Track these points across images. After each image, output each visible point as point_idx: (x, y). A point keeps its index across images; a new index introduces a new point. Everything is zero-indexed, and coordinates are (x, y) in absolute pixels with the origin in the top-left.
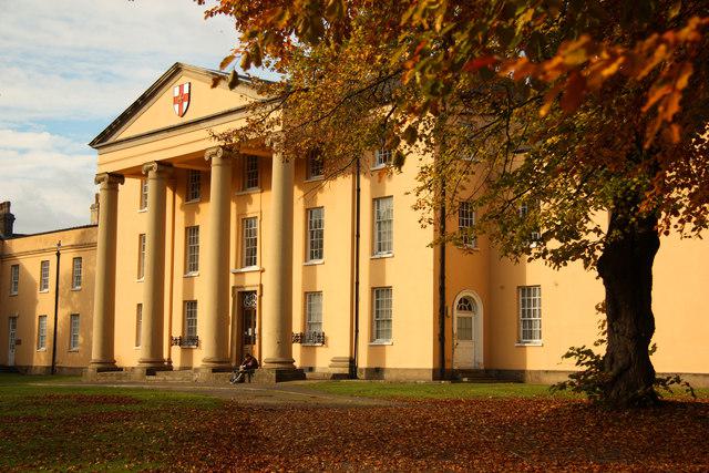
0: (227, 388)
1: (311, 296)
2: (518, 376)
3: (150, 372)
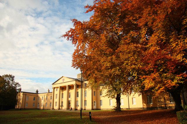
0: (68, 111)
1: (62, 102)
2: (100, 109)
3: (59, 109)
